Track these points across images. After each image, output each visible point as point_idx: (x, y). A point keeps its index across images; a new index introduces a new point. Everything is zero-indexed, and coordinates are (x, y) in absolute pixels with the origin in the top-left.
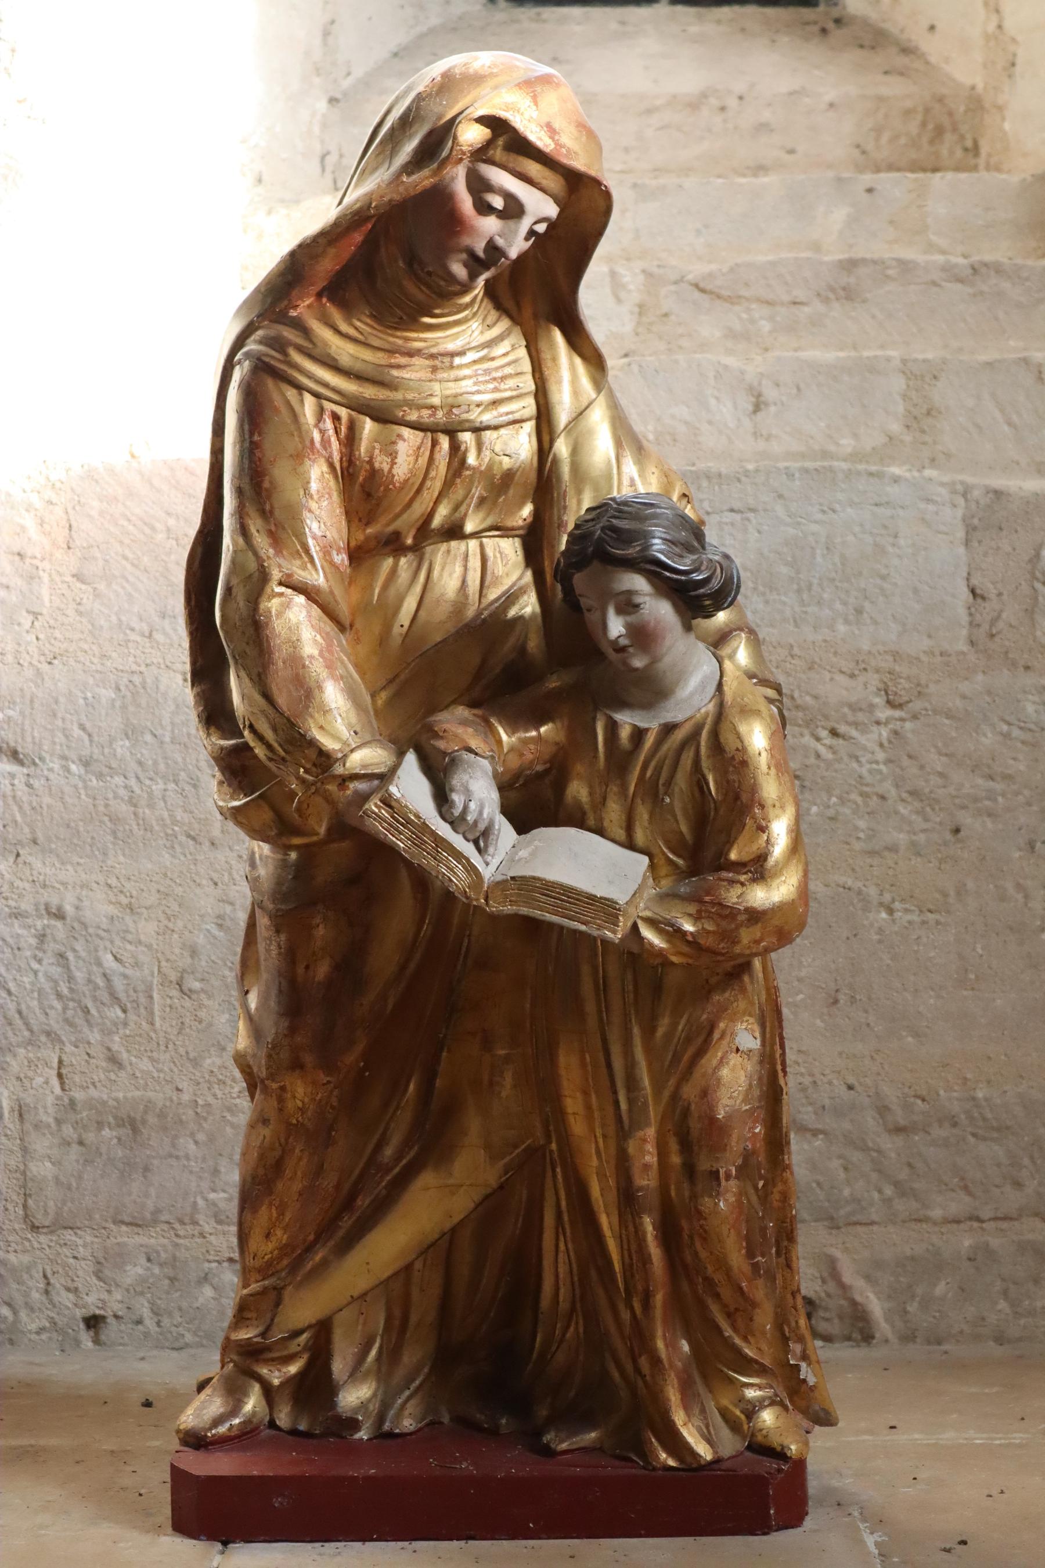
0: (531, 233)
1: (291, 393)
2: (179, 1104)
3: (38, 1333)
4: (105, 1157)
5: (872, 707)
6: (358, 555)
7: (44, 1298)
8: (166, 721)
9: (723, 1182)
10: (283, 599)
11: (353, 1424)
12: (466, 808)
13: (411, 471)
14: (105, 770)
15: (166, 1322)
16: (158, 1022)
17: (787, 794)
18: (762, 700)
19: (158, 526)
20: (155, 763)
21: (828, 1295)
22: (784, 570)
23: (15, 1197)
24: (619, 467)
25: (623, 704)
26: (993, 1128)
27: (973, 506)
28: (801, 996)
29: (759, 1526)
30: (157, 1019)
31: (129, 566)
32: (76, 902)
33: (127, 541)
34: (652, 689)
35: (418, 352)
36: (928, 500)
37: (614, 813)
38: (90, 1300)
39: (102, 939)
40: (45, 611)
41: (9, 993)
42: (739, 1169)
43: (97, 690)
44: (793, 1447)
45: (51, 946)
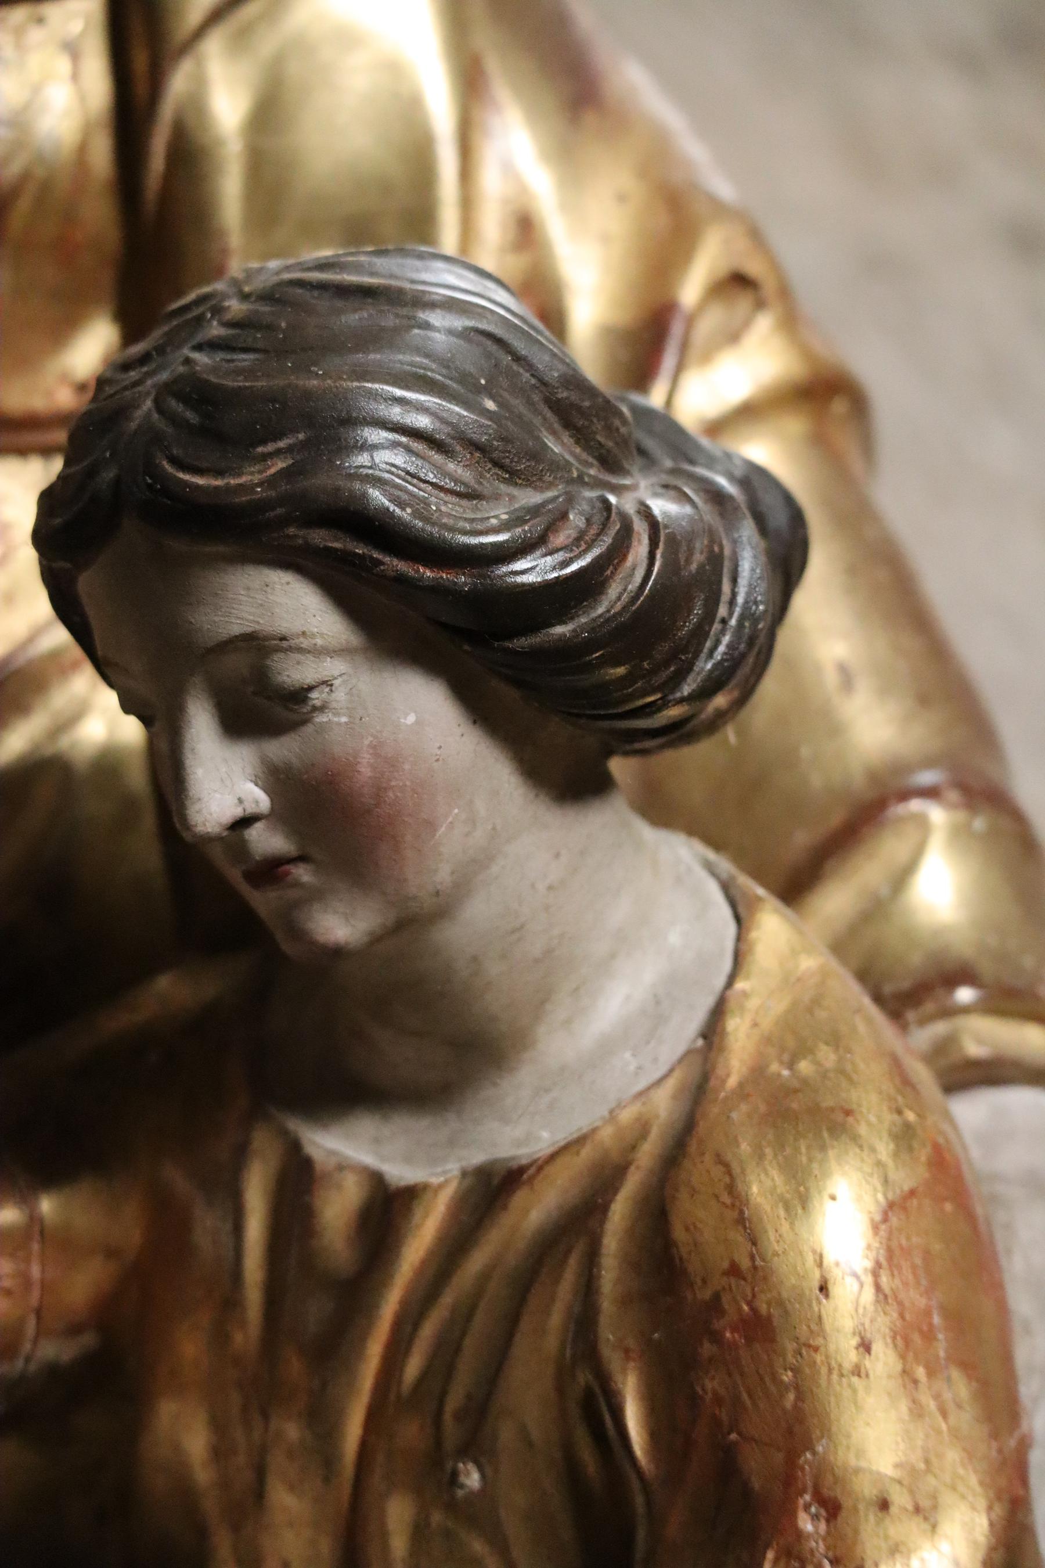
17: (953, 1456)
25: (349, 1093)
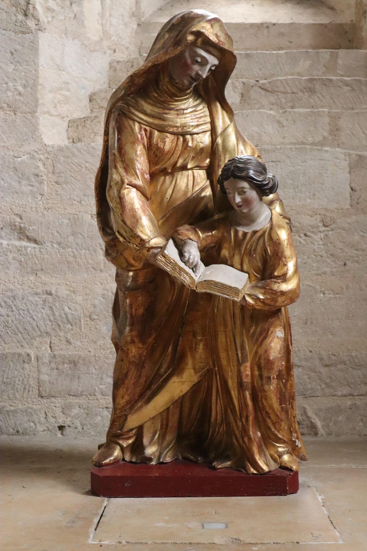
0: (210, 70)
1: (131, 122)
2: (90, 356)
3: (43, 431)
4: (65, 373)
5: (318, 227)
6: (153, 176)
7: (45, 420)
8: (85, 230)
9: (272, 380)
10: (129, 189)
11: (150, 459)
12: (189, 258)
13: (170, 148)
14: (65, 246)
15: (85, 428)
16: (83, 330)
18: (285, 223)
19: (83, 166)
20: (82, 244)
21: (303, 420)
22: (290, 181)
23: (35, 387)
24: (237, 147)
25: (239, 225)
26: (358, 366)
27: (352, 160)
28: (295, 322)
29: (284, 492)
30: (82, 328)
31: (73, 179)
32: (56, 290)
33: (72, 171)
34: (250, 219)
35: (172, 109)
36: (337, 158)
37: (237, 260)
38: (60, 420)
39: (64, 302)
40: (45, 194)
41: (34, 320)
42: (277, 376)
43: (63, 220)
44: (294, 467)
45: (47, 304)
